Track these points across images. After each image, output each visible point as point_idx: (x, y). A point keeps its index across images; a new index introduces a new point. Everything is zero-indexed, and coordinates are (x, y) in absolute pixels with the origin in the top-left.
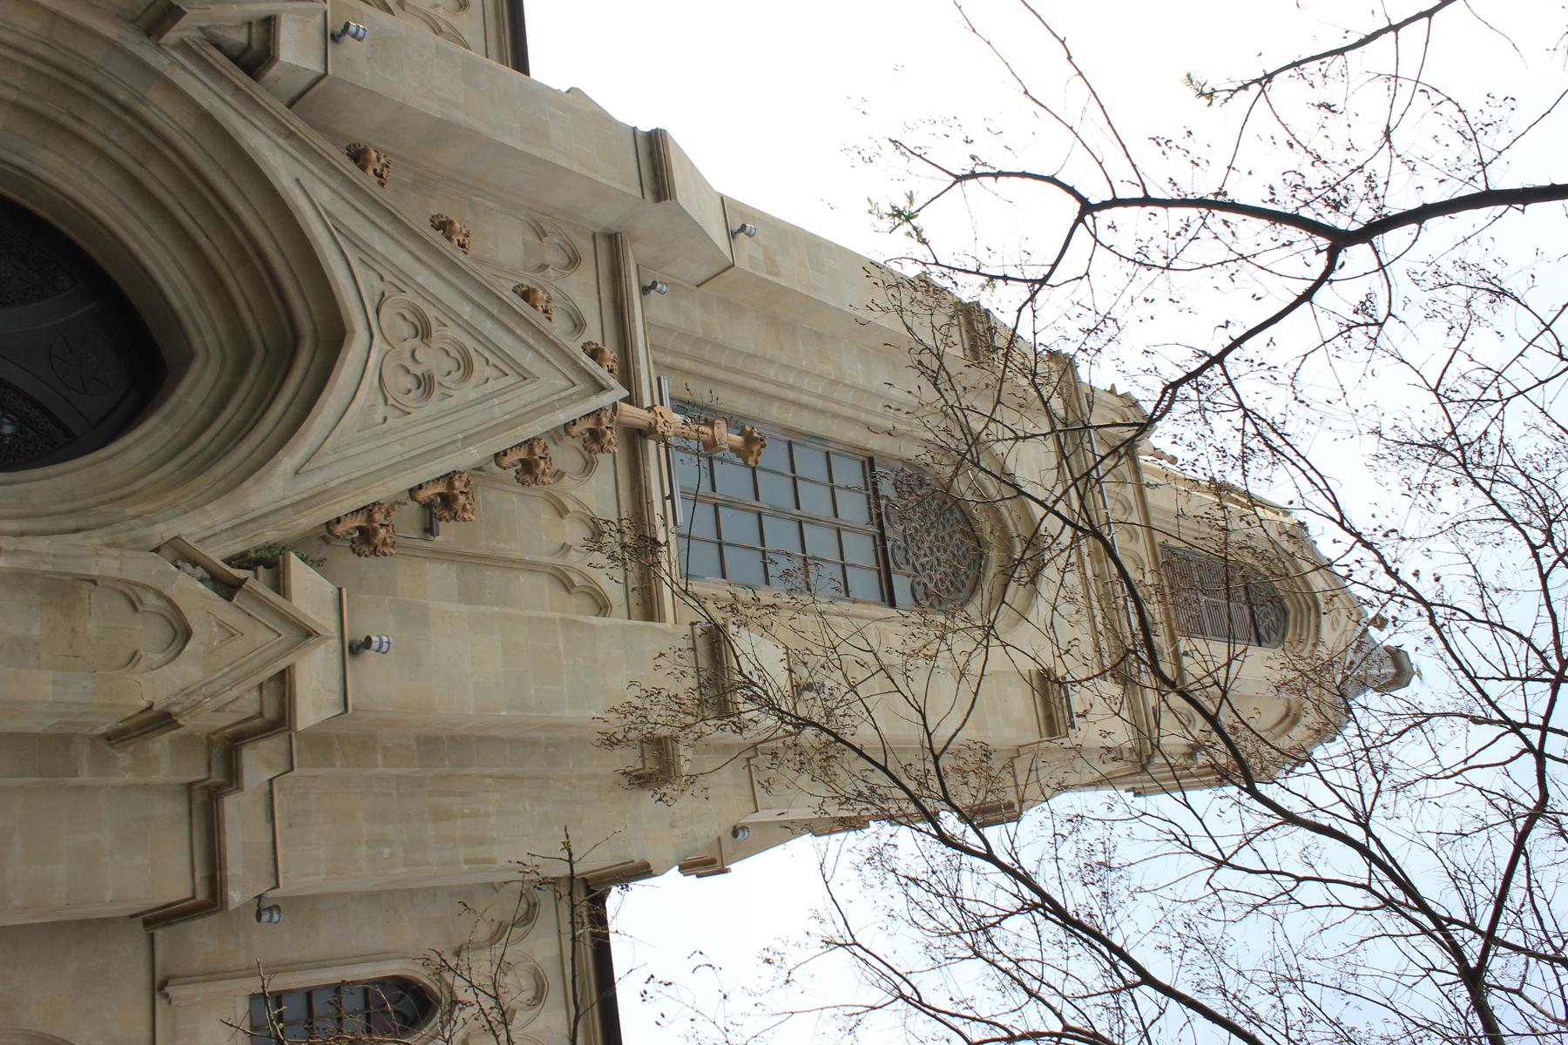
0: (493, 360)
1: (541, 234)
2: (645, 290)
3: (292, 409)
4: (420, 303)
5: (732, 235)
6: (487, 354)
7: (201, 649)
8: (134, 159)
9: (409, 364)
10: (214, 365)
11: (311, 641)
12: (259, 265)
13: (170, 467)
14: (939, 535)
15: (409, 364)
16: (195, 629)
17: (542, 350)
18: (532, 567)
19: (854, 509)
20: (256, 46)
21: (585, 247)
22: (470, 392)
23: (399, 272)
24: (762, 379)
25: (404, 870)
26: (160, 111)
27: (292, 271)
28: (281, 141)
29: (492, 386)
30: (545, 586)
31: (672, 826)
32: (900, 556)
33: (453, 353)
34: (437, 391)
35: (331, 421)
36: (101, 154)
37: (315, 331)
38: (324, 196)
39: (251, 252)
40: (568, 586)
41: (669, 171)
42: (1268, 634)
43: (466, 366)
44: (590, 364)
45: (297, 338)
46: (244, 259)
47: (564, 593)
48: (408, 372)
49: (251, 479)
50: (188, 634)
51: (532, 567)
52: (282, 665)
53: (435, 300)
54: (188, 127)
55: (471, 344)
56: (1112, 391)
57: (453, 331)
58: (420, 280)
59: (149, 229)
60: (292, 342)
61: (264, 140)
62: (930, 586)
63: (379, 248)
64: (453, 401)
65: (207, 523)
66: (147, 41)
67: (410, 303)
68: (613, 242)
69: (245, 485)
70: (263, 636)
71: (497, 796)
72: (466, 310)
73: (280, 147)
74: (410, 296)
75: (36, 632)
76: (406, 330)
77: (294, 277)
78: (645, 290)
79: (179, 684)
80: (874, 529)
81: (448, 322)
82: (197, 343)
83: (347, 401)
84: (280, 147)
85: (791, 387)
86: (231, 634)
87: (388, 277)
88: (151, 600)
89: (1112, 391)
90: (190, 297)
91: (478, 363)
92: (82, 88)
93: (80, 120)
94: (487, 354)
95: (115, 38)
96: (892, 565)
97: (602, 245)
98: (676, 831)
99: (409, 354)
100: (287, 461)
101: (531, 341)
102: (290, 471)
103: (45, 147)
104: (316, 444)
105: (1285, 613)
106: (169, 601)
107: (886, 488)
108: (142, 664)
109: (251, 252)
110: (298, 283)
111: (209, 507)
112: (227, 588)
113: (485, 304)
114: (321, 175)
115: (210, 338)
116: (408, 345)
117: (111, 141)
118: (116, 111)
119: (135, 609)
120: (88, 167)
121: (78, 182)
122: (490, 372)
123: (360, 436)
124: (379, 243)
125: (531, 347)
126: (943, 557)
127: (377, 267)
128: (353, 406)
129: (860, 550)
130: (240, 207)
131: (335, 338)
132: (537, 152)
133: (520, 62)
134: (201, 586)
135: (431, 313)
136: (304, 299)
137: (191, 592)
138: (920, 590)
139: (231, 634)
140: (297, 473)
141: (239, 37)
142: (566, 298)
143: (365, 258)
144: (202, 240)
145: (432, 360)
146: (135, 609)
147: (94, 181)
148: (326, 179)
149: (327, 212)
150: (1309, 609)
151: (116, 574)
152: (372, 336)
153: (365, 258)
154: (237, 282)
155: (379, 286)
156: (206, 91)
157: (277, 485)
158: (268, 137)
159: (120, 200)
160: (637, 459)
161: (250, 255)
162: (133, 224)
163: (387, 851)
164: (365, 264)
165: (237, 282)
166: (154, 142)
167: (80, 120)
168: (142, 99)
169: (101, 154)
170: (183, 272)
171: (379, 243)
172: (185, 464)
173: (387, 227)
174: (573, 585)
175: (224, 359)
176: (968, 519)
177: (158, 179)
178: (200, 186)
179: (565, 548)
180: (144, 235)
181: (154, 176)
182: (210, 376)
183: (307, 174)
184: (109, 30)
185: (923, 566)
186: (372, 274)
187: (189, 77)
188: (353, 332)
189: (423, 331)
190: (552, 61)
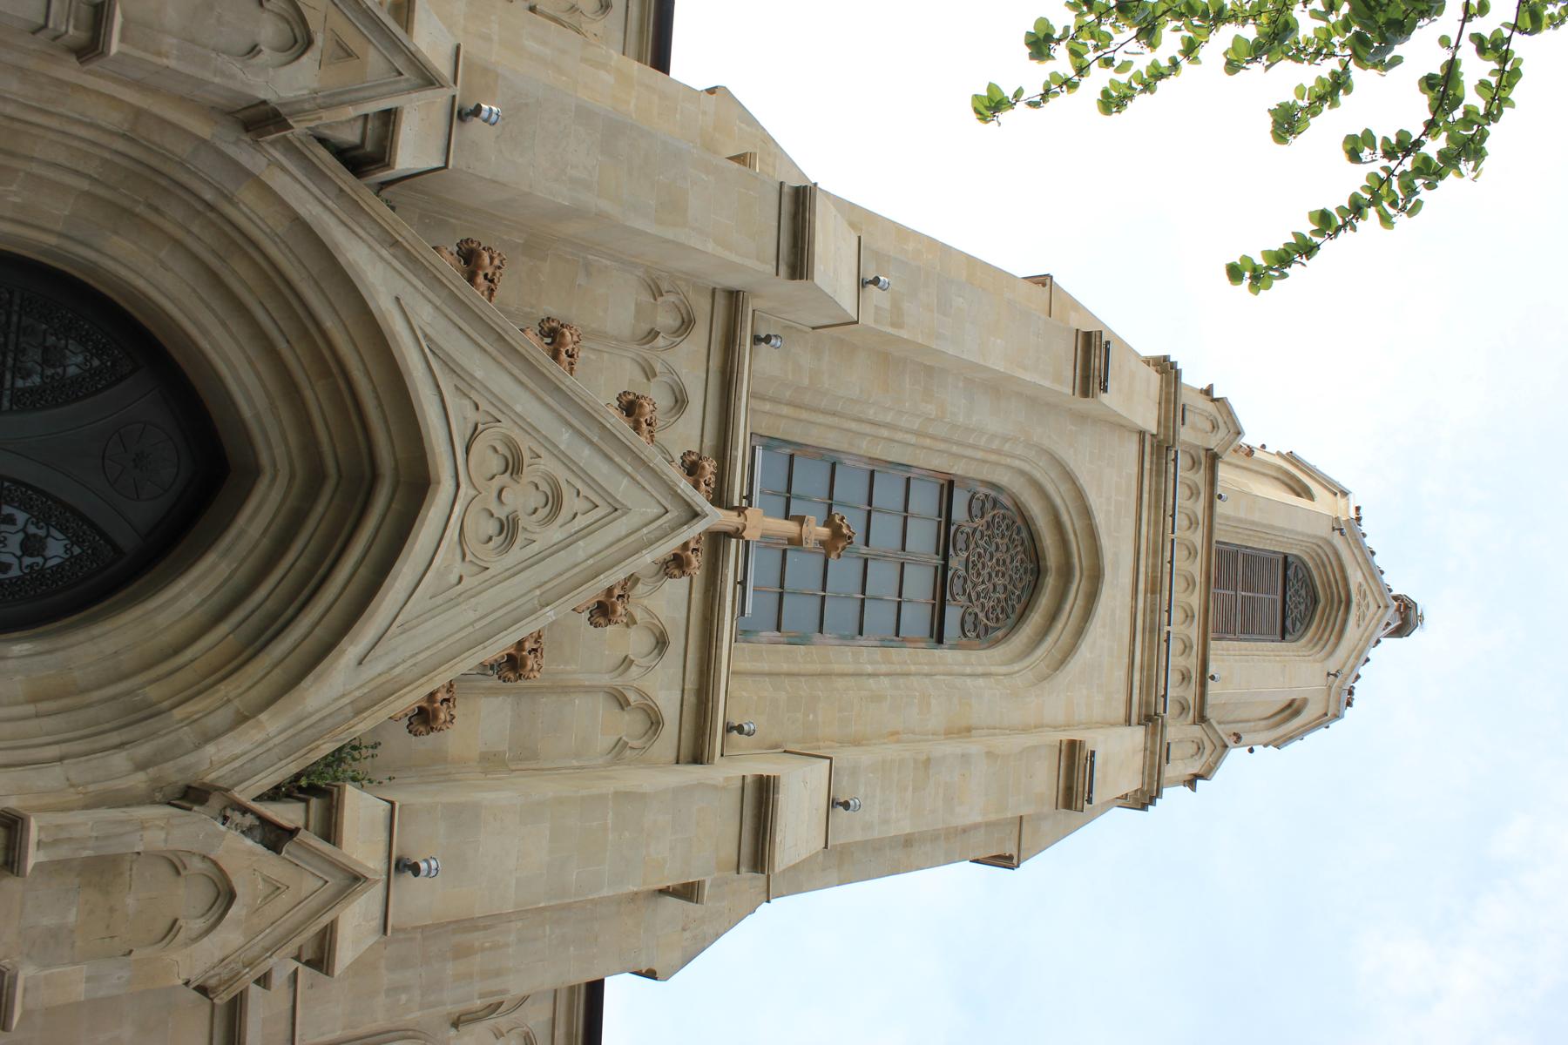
0: (584, 491)
1: (657, 292)
2: (757, 340)
3: (362, 571)
4: (517, 435)
5: (862, 284)
6: (579, 485)
7: (244, 912)
8: (214, 252)
9: (494, 506)
10: (282, 480)
11: (359, 887)
12: (342, 385)
13: (224, 628)
14: (997, 567)
15: (494, 506)
16: (239, 890)
17: (639, 478)
18: (589, 690)
19: (923, 537)
20: (369, 147)
21: (701, 307)
22: (555, 533)
23: (497, 401)
24: (860, 420)
25: (419, 1014)
26: (249, 210)
27: (378, 398)
28: (384, 253)
29: (581, 521)
30: (602, 707)
31: (684, 930)
32: (958, 583)
33: (544, 487)
34: (521, 537)
35: (403, 596)
36: (178, 244)
37: (396, 469)
38: (424, 314)
39: (335, 370)
40: (622, 703)
41: (811, 243)
42: (1294, 625)
43: (555, 501)
44: (684, 485)
45: (375, 477)
46: (326, 373)
47: (617, 710)
48: (492, 515)
49: (311, 677)
50: (232, 896)
51: (589, 690)
52: (325, 920)
53: (531, 430)
54: (279, 230)
55: (561, 474)
56: (1208, 392)
57: (548, 464)
58: (518, 408)
59: (224, 324)
60: (368, 486)
61: (366, 250)
62: (981, 616)
63: (479, 374)
64: (535, 547)
65: (260, 737)
66: (246, 138)
67: (507, 437)
68: (734, 298)
69: (303, 684)
70: (310, 884)
71: (519, 924)
72: (564, 438)
73: (381, 257)
74: (506, 427)
75: (72, 917)
76: (496, 464)
77: (380, 405)
78: (757, 340)
79: (218, 955)
80: (938, 561)
81: (542, 452)
82: (264, 459)
83: (422, 569)
84: (381, 257)
85: (886, 426)
86: (276, 889)
87: (483, 405)
88: (197, 865)
89: (1208, 392)
90: (261, 403)
91: (570, 503)
92: (164, 183)
93: (156, 210)
94: (579, 485)
95: (207, 137)
96: (948, 597)
97: (721, 302)
98: (687, 934)
99: (495, 494)
100: (352, 649)
101: (629, 469)
102: (354, 662)
103: (116, 233)
104: (385, 624)
105: (1315, 601)
106: (215, 863)
107: (959, 513)
108: (181, 936)
109: (335, 370)
110: (383, 411)
111: (263, 717)
112: (275, 837)
113: (585, 430)
114: (426, 291)
115: (279, 451)
116: (496, 484)
117: (189, 232)
118: (200, 207)
119: (178, 873)
120: (162, 254)
121: (147, 269)
122: (579, 504)
123: (437, 600)
124: (478, 366)
125: (628, 474)
126: (1000, 581)
127: (474, 395)
128: (429, 574)
129: (920, 583)
130: (329, 323)
131: (418, 487)
132: (669, 234)
133: (661, 61)
134: (249, 842)
135: (525, 444)
136: (388, 431)
137: (239, 852)
138: (969, 619)
139: (276, 889)
140: (360, 663)
141: (350, 136)
142: (672, 371)
143: (462, 386)
144: (282, 346)
145: (521, 498)
146: (178, 873)
147: (167, 269)
148: (431, 295)
149: (426, 336)
150: (1340, 602)
151: (161, 846)
152: (458, 486)
153: (462, 386)
154: (315, 395)
155: (473, 416)
156: (304, 194)
157: (340, 679)
158: (370, 247)
159: (194, 290)
160: (717, 560)
161: (332, 369)
162: (207, 319)
163: (404, 997)
164: (458, 386)
165: (315, 395)
166: (240, 241)
167: (156, 210)
168: (229, 199)
169: (178, 244)
170: (257, 374)
171: (478, 366)
172: (239, 624)
173: (489, 348)
174: (629, 704)
175: (292, 477)
176: (1033, 537)
177: (239, 275)
178: (286, 292)
179: (626, 662)
180: (217, 331)
181: (234, 272)
182: (275, 496)
183: (409, 289)
184: (202, 128)
185: (978, 595)
186: (466, 402)
187: (287, 179)
188: (439, 483)
189: (514, 466)
190: (692, 62)
